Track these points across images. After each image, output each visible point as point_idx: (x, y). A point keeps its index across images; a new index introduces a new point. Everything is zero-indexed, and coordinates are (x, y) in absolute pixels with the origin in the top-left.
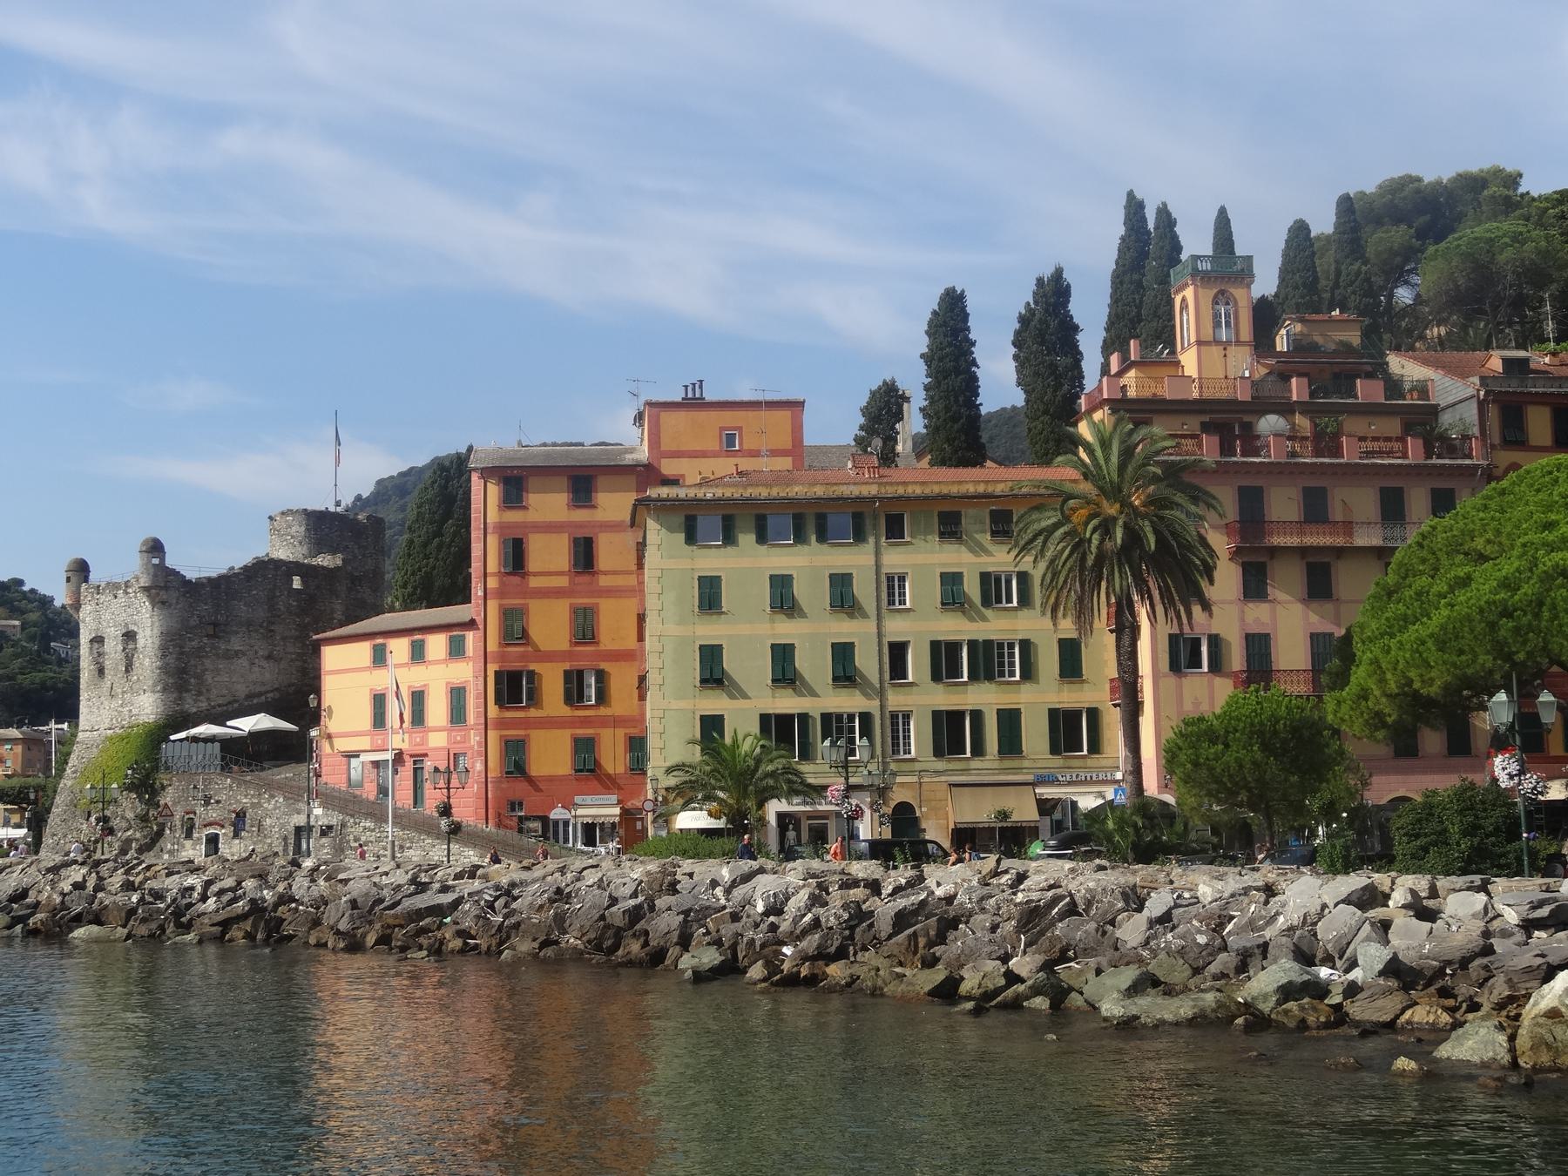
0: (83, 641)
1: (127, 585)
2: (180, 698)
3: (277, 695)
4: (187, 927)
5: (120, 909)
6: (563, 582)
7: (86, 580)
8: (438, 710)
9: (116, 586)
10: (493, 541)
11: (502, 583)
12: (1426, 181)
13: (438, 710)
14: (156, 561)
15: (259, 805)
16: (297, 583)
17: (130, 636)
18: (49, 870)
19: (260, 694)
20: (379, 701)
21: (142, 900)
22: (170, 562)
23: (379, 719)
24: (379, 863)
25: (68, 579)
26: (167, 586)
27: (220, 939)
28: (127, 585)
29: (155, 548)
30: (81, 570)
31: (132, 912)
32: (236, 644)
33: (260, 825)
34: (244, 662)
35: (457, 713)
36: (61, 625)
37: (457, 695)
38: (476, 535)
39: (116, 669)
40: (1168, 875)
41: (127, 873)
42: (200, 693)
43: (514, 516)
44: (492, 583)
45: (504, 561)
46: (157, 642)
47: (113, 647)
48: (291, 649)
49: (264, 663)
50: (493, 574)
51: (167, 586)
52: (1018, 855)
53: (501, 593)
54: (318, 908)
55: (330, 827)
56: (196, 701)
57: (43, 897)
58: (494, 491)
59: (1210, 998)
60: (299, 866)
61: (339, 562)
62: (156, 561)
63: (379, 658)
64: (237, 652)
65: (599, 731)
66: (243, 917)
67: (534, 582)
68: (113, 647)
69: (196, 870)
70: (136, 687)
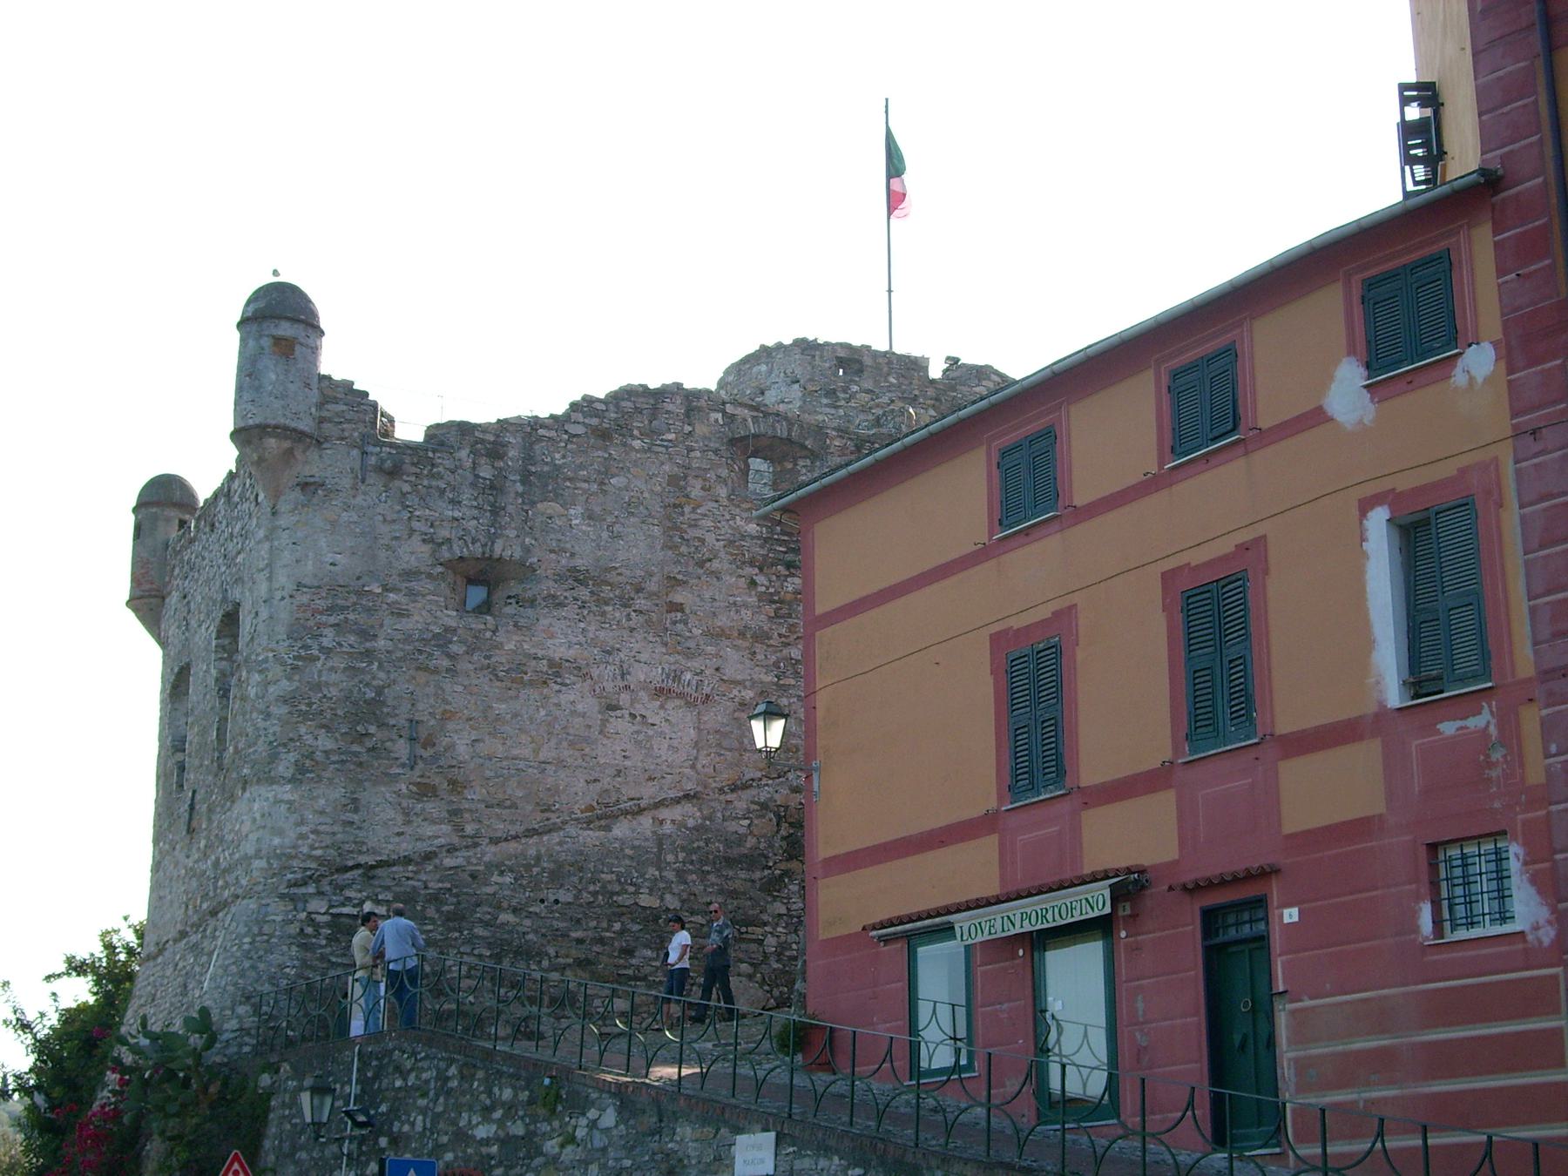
2: (355, 804)
3: (689, 813)
20: (1034, 682)
34: (577, 699)
64: (556, 667)
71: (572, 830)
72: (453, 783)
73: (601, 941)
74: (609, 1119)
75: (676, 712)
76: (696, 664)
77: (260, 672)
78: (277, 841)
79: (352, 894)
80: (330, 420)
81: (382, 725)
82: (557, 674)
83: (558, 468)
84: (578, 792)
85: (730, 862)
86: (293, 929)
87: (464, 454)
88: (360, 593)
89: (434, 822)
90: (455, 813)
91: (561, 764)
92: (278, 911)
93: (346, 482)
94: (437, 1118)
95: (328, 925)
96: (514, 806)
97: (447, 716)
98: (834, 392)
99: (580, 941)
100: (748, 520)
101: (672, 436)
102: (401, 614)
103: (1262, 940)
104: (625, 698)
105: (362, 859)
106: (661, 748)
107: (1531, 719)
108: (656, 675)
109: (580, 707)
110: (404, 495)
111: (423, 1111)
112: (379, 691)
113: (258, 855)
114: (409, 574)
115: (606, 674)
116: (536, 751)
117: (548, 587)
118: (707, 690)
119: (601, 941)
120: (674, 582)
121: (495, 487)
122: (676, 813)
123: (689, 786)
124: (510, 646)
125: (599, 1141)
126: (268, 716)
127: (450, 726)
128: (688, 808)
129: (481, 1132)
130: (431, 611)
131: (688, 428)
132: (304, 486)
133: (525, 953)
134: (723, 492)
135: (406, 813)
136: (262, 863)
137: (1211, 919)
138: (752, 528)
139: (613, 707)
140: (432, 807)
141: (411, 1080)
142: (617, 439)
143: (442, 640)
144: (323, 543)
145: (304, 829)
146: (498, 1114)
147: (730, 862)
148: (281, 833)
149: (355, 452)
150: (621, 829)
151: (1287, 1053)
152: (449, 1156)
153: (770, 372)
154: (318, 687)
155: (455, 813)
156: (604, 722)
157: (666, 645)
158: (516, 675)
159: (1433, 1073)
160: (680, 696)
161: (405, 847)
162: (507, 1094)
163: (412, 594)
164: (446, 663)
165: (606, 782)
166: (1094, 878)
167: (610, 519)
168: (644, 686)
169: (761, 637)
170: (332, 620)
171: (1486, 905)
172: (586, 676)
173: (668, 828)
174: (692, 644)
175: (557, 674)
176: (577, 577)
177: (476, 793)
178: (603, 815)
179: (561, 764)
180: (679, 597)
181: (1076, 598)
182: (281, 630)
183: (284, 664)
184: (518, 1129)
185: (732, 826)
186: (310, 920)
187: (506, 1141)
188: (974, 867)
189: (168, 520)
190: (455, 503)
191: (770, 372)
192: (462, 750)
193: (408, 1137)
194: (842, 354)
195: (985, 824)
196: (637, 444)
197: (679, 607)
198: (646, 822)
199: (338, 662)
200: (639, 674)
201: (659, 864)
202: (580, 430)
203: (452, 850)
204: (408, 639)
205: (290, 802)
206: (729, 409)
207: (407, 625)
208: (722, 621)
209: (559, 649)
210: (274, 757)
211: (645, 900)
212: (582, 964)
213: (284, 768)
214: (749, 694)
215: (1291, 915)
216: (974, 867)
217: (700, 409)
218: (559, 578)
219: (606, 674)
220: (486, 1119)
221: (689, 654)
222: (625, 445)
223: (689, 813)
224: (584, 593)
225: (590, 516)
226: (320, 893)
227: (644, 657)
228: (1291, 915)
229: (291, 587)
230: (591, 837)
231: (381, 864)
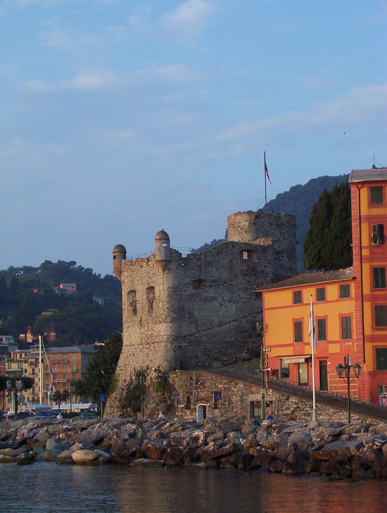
0: (123, 293)
1: (148, 260)
3: (235, 323)
4: (198, 459)
5: (157, 449)
7: (124, 257)
8: (334, 330)
9: (142, 260)
10: (365, 227)
11: (372, 253)
12: (102, 277)
13: (334, 330)
14: (165, 245)
15: (229, 389)
16: (245, 256)
17: (151, 289)
18: (115, 426)
20: (298, 326)
21: (169, 443)
22: (173, 245)
23: (299, 336)
24: (314, 424)
25: (115, 257)
26: (171, 260)
27: (218, 467)
28: (148, 260)
29: (164, 237)
30: (121, 251)
31: (164, 451)
33: (230, 400)
34: (216, 304)
35: (346, 333)
36: (112, 285)
37: (345, 322)
38: (354, 224)
41: (159, 428)
43: (377, 211)
44: (365, 252)
46: (166, 293)
47: (141, 297)
50: (366, 247)
51: (171, 260)
53: (371, 259)
54: (273, 450)
55: (271, 402)
57: (112, 442)
58: (364, 192)
60: (259, 425)
61: (270, 243)
62: (165, 245)
63: (298, 299)
66: (229, 454)
68: (141, 297)
69: (199, 427)
71: (216, 328)
73: (222, 348)
76: (235, 295)
84: (216, 321)
85: (243, 332)
86: (172, 348)
88: (179, 288)
94: (212, 384)
97: (194, 309)
102: (186, 291)
103: (326, 365)
104: (223, 303)
107: (355, 344)
114: (187, 284)
115: (220, 299)
119: (222, 348)
120: (231, 280)
121: (200, 266)
123: (235, 318)
125: (240, 388)
128: (235, 322)
129: (220, 386)
130: (190, 290)
133: (209, 351)
134: (239, 262)
135: (188, 326)
137: (320, 362)
138: (245, 268)
140: (193, 326)
143: (193, 295)
147: (243, 332)
150: (224, 327)
151: (329, 380)
158: (205, 300)
161: (189, 333)
163: (187, 287)
164: (193, 299)
169: (247, 289)
172: (216, 299)
173: (232, 326)
176: (214, 281)
177: (200, 322)
180: (232, 283)
184: (227, 386)
185: (242, 325)
186: (175, 347)
187: (225, 388)
188: (290, 351)
192: (197, 315)
195: (291, 345)
197: (232, 285)
198: (228, 325)
200: (226, 298)
202: (214, 253)
203: (196, 333)
204: (187, 295)
208: (240, 287)
209: (212, 295)
212: (219, 352)
214: (245, 300)
215: (329, 363)
216: (290, 351)
218: (212, 282)
219: (220, 299)
220: (221, 384)
223: (235, 323)
224: (216, 284)
225: (216, 269)
230: (219, 329)
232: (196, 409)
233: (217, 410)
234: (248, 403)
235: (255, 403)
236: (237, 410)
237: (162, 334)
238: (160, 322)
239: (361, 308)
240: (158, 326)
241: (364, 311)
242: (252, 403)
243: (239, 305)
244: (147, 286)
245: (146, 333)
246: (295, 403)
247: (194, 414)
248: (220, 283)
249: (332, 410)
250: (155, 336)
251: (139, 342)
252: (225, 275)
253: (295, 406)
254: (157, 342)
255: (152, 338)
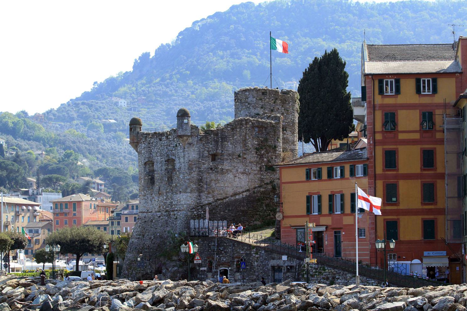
2: (200, 196)
3: (248, 193)
6: (417, 136)
11: (384, 137)
19: (239, 194)
32: (226, 166)
34: (230, 176)
39: (161, 179)
40: (284, 264)
42: (209, 193)
45: (385, 124)
48: (254, 168)
49: (241, 176)
50: (378, 132)
52: (233, 151)
55: (291, 267)
56: (207, 197)
59: (380, 35)
64: (227, 170)
65: (436, 217)
67: (401, 136)
70: (174, 190)
72: (213, 191)
74: (263, 252)
75: (245, 176)
77: (183, 174)
78: (188, 202)
79: (200, 210)
80: (193, 132)
81: (202, 183)
82: (227, 172)
83: (226, 136)
87: (212, 136)
89: (210, 198)
90: (213, 196)
91: (228, 187)
92: (189, 214)
93: (195, 143)
95: (197, 215)
96: (222, 194)
97: (211, 181)
98: (262, 99)
99: (233, 216)
100: (256, 141)
101: (243, 128)
104: (237, 175)
105: (201, 205)
106: (243, 183)
108: (242, 170)
109: (231, 177)
110: (204, 144)
111: (231, 249)
112: (202, 177)
113: (185, 204)
115: (234, 171)
116: (224, 185)
117: (226, 157)
118: (249, 172)
122: (245, 194)
124: (220, 168)
126: (185, 182)
127: (212, 182)
129: (242, 252)
130: (208, 164)
131: (246, 126)
132: (189, 144)
136: (186, 206)
139: (235, 177)
140: (210, 196)
141: (228, 244)
142: (235, 129)
144: (193, 153)
145: (192, 200)
146: (245, 250)
148: (189, 201)
149: (197, 138)
151: (282, 234)
152: (236, 255)
153: (249, 94)
154: (193, 177)
155: (213, 196)
156: (234, 179)
157: (243, 165)
159: (423, 86)
160: (246, 174)
162: (246, 248)
165: (235, 189)
166: (323, 225)
167: (234, 144)
168: (240, 172)
170: (195, 166)
171: (409, 121)
174: (247, 164)
175: (227, 172)
177: (216, 193)
178: (235, 194)
179: (228, 187)
181: (320, 191)
182: (187, 168)
183: (187, 174)
184: (248, 252)
189: (138, 127)
190: (211, 144)
191: (249, 94)
193: (228, 252)
194: (263, 91)
196: (238, 130)
197: (245, 158)
198: (241, 195)
199: (196, 173)
200: (239, 170)
201: (244, 202)
205: (190, 196)
206: (252, 121)
207: (205, 166)
210: (187, 189)
211: (242, 208)
213: (189, 190)
215: (344, 233)
217: (248, 122)
219: (234, 171)
220: (243, 250)
221: (247, 166)
222: (236, 130)
226: (195, 211)
227: (240, 167)
228: (344, 233)
229: (188, 161)
231: (203, 205)
232: (217, 272)
233: (238, 274)
234: (269, 267)
235: (276, 268)
236: (259, 274)
237: (183, 203)
238: (180, 192)
239: (374, 185)
240: (178, 196)
241: (377, 188)
242: (273, 267)
243: (251, 176)
244: (166, 159)
245: (164, 201)
246: (315, 268)
247: (215, 277)
248: (234, 157)
249: (350, 275)
250: (174, 205)
251: (156, 210)
252: (239, 149)
253: (314, 271)
254: (177, 210)
255: (172, 206)
